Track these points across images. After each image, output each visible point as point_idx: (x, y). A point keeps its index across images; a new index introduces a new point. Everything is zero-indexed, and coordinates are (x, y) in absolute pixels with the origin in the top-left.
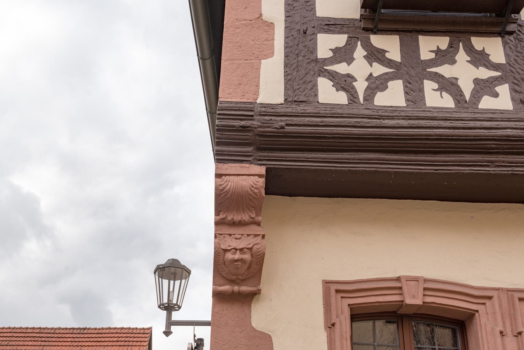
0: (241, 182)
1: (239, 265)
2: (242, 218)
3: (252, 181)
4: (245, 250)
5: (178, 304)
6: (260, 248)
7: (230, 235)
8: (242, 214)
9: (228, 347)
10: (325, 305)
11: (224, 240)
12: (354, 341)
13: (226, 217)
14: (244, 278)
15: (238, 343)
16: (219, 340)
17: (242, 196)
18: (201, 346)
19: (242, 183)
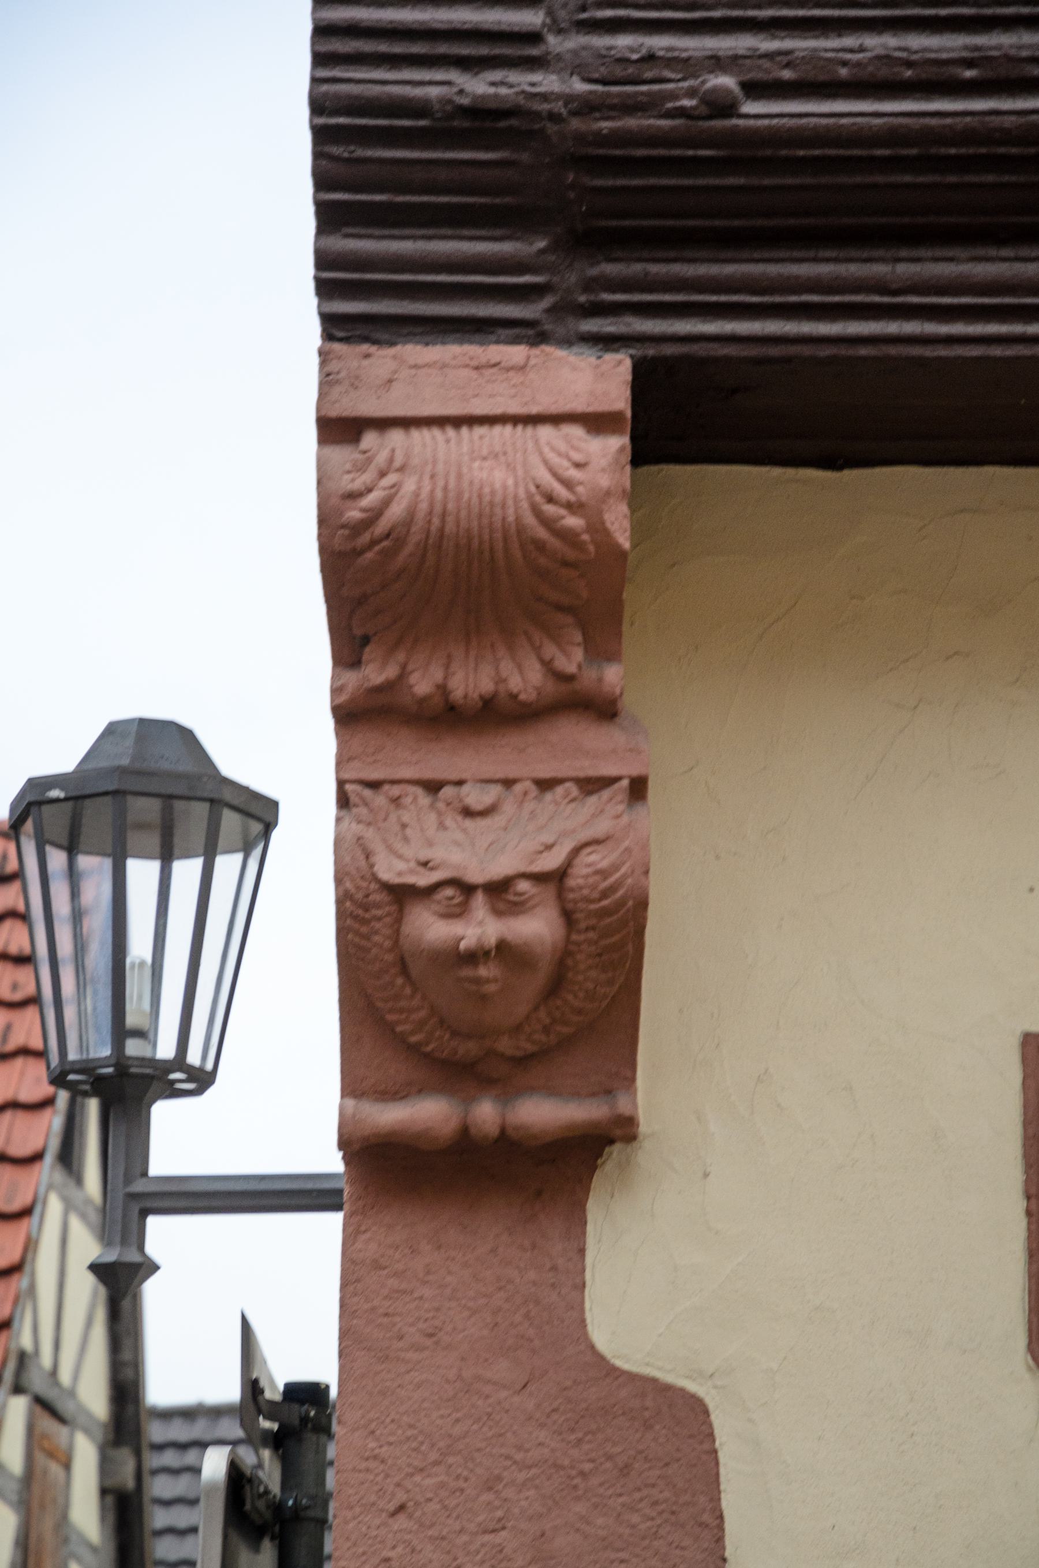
0: (481, 469)
1: (488, 981)
2: (497, 683)
3: (546, 462)
4: (523, 886)
6: (615, 867)
7: (433, 787)
8: (502, 651)
9: (442, 1485)
10: (1033, 1201)
11: (393, 818)
13: (403, 675)
14: (530, 1048)
15: (508, 1457)
16: (390, 1444)
17: (487, 554)
18: (310, 1438)
19: (484, 475)
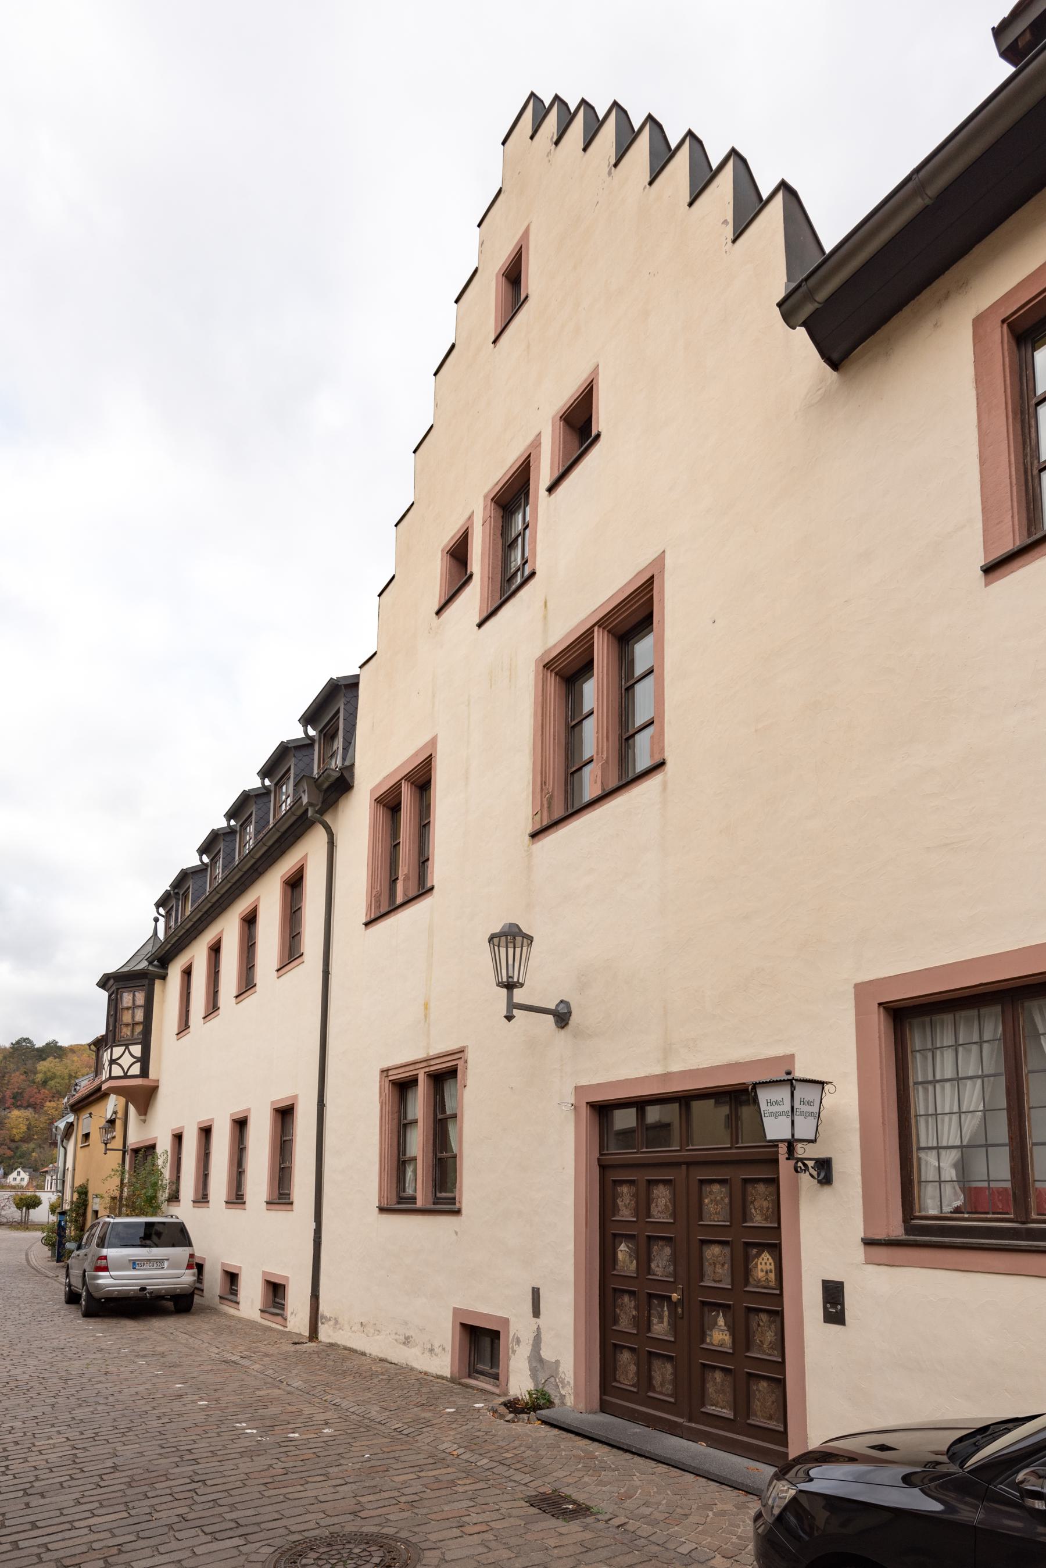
5: (520, 981)
12: (696, 1105)
